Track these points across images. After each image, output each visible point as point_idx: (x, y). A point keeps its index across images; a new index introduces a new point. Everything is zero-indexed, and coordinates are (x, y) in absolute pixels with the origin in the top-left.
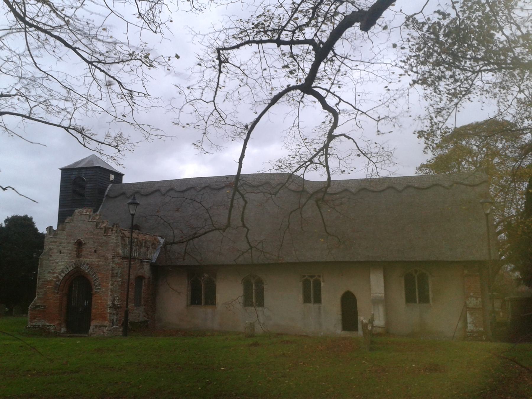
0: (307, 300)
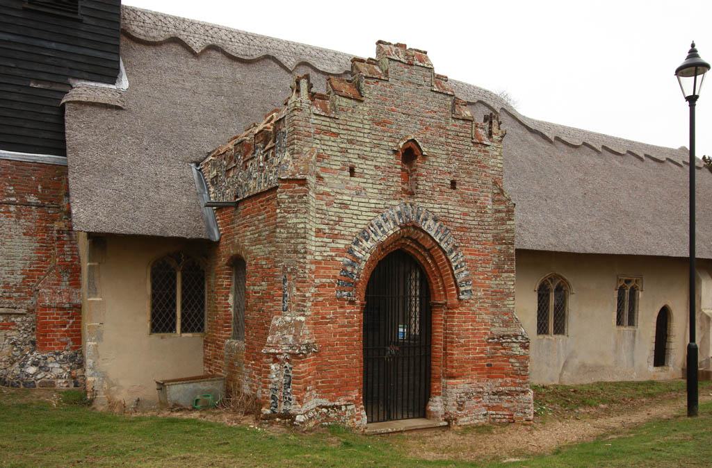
0: (619, 322)
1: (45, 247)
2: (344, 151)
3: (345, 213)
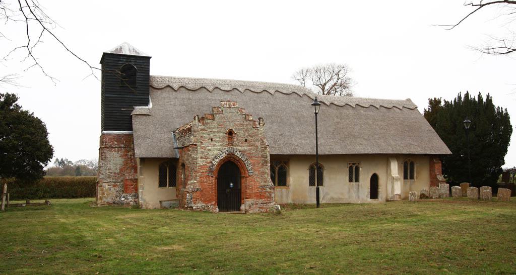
0: (351, 180)
1: (126, 160)
3: (210, 151)
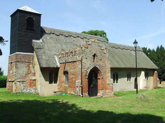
0: (128, 81)
2: (85, 56)
